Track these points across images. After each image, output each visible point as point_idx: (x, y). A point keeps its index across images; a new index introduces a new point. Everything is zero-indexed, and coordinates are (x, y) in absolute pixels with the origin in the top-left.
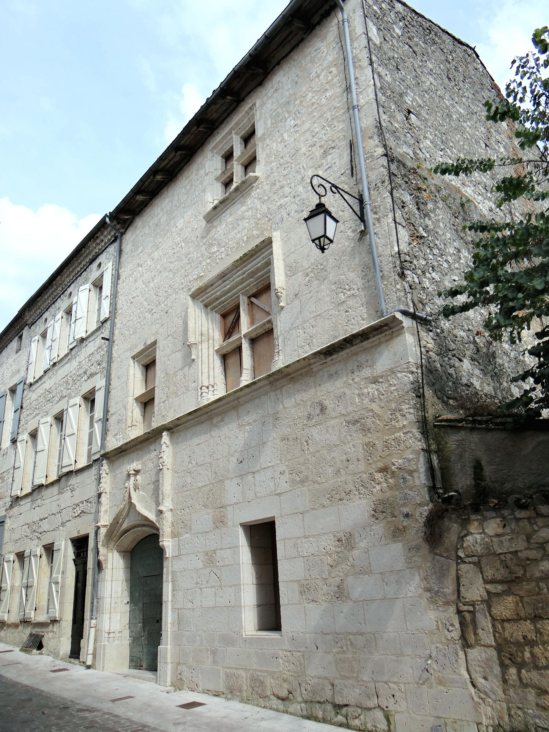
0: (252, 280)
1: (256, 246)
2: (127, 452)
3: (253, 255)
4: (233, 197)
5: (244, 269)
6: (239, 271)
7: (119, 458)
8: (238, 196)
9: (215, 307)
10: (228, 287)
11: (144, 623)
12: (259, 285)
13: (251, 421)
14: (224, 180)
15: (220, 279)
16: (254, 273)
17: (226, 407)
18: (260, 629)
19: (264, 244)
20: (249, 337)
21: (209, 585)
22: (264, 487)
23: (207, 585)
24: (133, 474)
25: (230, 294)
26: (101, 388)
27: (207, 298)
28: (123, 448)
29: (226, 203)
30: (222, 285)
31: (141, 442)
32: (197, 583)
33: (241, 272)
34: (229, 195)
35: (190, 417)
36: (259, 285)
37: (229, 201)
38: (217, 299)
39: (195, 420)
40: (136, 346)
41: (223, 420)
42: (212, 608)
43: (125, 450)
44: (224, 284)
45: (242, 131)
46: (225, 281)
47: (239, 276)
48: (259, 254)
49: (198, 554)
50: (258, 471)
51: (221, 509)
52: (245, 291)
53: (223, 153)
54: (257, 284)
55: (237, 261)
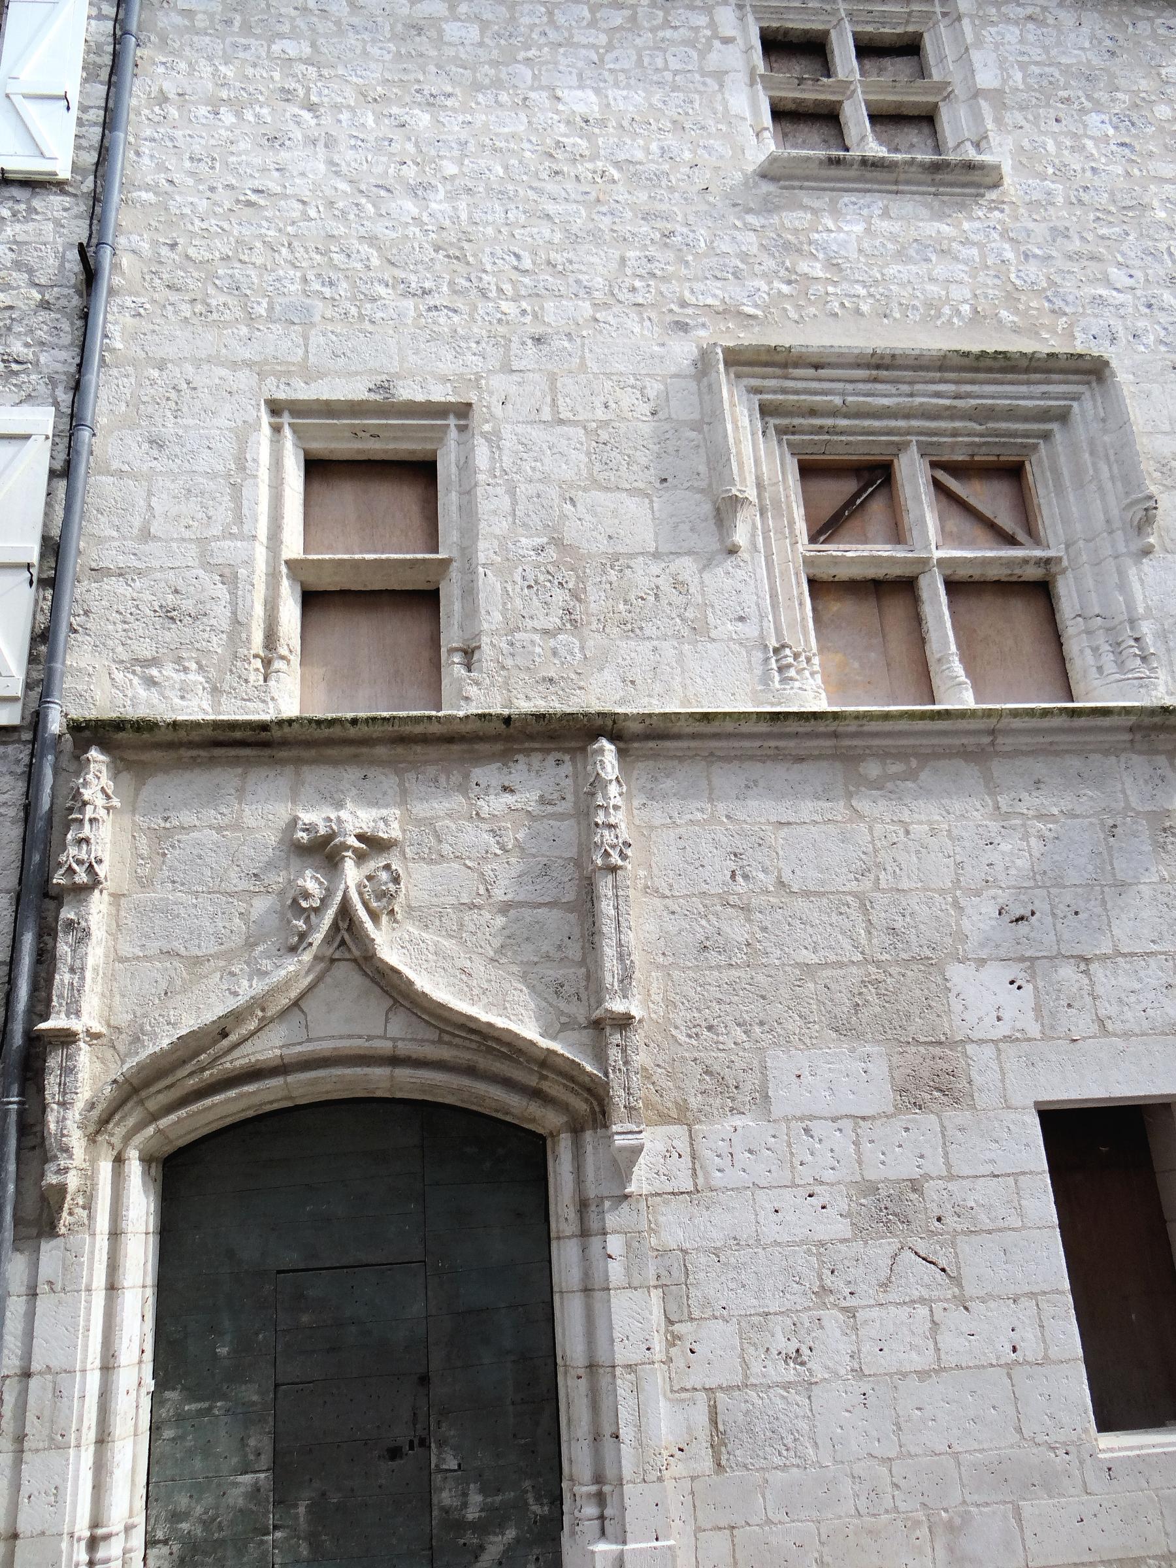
0: (977, 427)
1: (1051, 355)
2: (283, 754)
3: (1013, 369)
4: (902, 177)
5: (968, 388)
6: (946, 382)
7: (195, 763)
8: (919, 184)
9: (793, 430)
10: (886, 401)
11: (282, 1469)
12: (984, 450)
13: (1055, 811)
14: (781, 99)
15: (868, 366)
16: (990, 414)
17: (936, 741)
18: (1106, 1424)
19: (1072, 364)
20: (949, 572)
21: (893, 1296)
22: (1140, 1007)
23: (882, 1298)
24: (355, 850)
25: (877, 424)
26: (27, 437)
27: (784, 391)
28: (276, 733)
29: (877, 174)
30: (861, 386)
31: (449, 739)
32: (825, 1290)
33: (951, 388)
34: (906, 163)
35: (763, 727)
36: (984, 450)
37: (884, 175)
38: (813, 412)
39: (773, 743)
40: (310, 375)
41: (912, 776)
42: (923, 1375)
43: (284, 743)
44: (869, 386)
45: (867, 23)
46: (875, 380)
47: (938, 395)
48: (1038, 376)
49: (817, 1189)
50: (1104, 958)
51: (937, 1051)
52: (932, 444)
53: (775, 25)
54: (980, 445)
55: (966, 354)
